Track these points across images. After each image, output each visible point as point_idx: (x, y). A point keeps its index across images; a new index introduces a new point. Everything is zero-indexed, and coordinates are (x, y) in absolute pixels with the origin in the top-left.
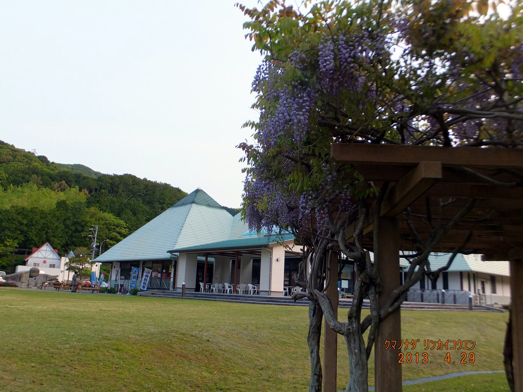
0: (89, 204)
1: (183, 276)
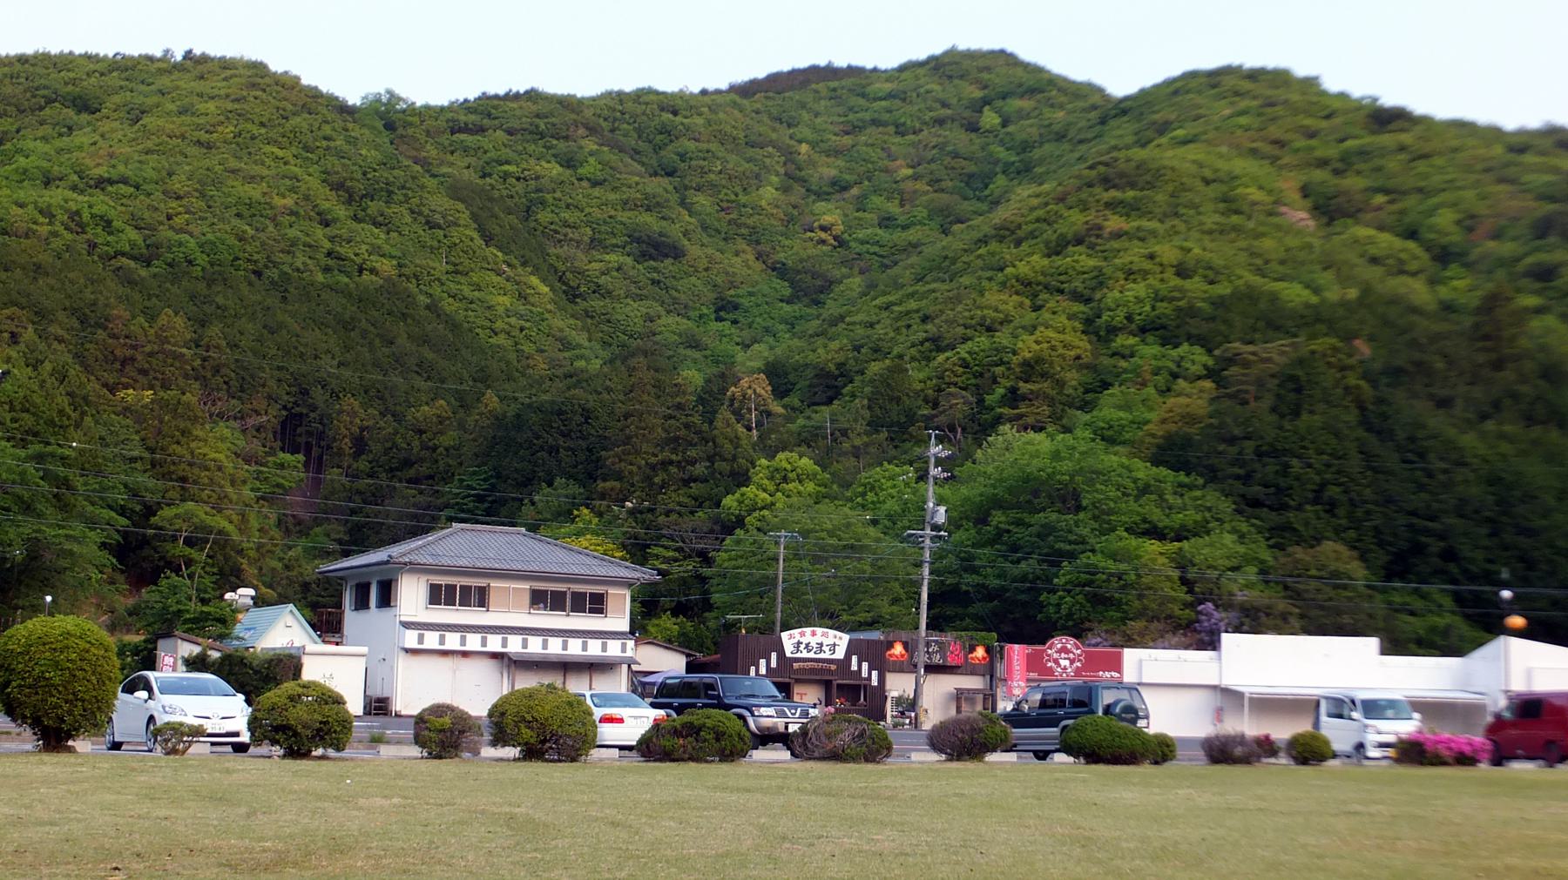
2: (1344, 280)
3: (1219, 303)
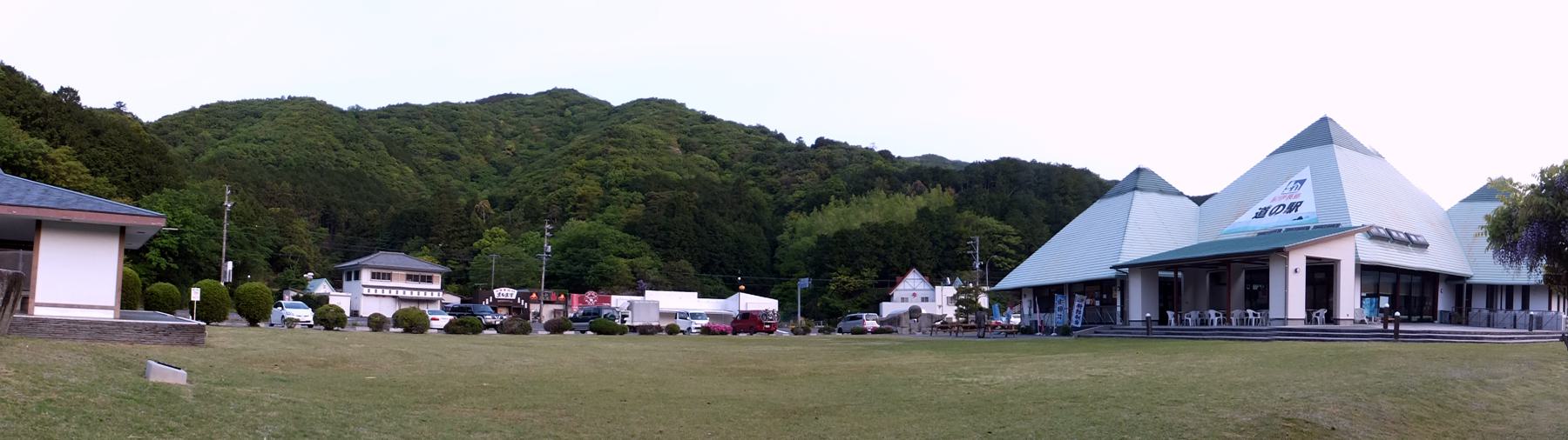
0: (959, 206)
1: (1138, 304)
2: (691, 172)
3: (647, 178)
